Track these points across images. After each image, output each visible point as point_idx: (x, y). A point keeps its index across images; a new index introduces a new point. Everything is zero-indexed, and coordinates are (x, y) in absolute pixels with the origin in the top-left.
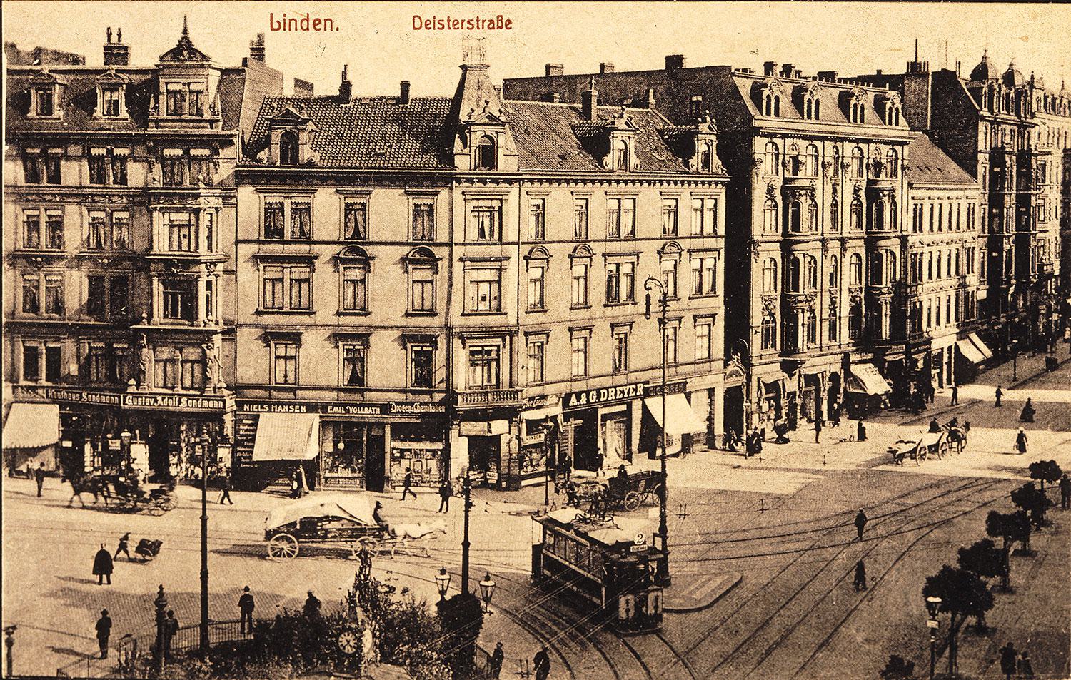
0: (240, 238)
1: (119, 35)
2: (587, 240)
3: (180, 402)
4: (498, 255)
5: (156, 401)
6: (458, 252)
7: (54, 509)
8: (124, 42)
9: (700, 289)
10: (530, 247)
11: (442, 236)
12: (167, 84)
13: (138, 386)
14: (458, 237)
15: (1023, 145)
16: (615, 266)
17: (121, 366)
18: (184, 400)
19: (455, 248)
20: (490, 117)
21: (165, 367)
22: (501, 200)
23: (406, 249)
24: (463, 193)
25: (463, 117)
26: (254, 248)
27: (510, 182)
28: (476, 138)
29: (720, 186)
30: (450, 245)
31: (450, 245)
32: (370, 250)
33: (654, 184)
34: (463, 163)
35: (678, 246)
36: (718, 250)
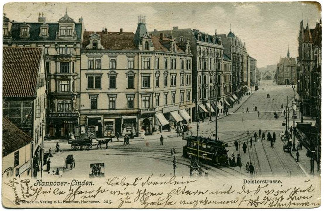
0: (81, 69)
1: (43, 15)
2: (115, 69)
3: (65, 115)
4: (149, 73)
5: (58, 115)
6: (140, 71)
7: (151, 139)
8: (44, 16)
9: (183, 83)
10: (164, 71)
11: (136, 68)
12: (61, 27)
13: (52, 111)
14: (140, 68)
15: (62, 33)
16: (79, 77)
17: (232, 97)
18: (66, 115)
19: (153, 71)
20: (148, 36)
21: (60, 105)
22: (150, 58)
23: (127, 71)
24: (141, 56)
25: (141, 36)
26: (86, 72)
27: (152, 53)
28: (144, 42)
29: (135, 54)
30: (138, 70)
31: (138, 70)
32: (117, 71)
33: (162, 54)
34: (141, 48)
35: (184, 72)
36: (191, 74)
